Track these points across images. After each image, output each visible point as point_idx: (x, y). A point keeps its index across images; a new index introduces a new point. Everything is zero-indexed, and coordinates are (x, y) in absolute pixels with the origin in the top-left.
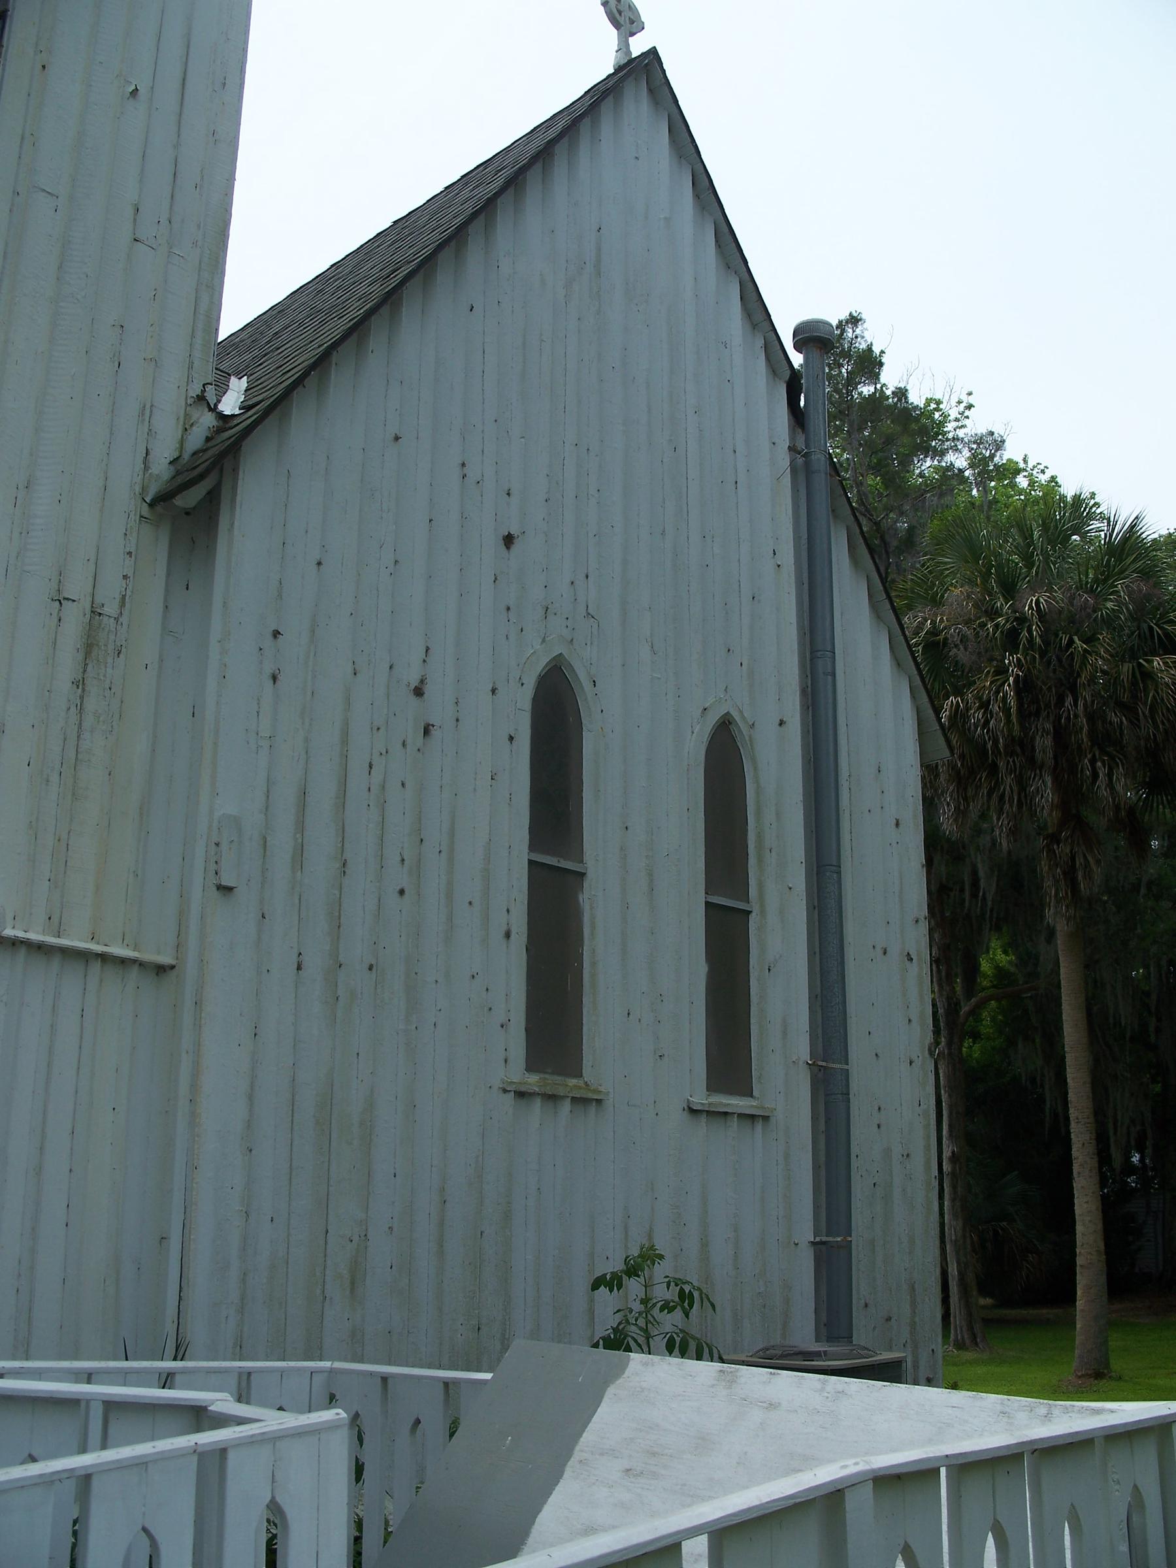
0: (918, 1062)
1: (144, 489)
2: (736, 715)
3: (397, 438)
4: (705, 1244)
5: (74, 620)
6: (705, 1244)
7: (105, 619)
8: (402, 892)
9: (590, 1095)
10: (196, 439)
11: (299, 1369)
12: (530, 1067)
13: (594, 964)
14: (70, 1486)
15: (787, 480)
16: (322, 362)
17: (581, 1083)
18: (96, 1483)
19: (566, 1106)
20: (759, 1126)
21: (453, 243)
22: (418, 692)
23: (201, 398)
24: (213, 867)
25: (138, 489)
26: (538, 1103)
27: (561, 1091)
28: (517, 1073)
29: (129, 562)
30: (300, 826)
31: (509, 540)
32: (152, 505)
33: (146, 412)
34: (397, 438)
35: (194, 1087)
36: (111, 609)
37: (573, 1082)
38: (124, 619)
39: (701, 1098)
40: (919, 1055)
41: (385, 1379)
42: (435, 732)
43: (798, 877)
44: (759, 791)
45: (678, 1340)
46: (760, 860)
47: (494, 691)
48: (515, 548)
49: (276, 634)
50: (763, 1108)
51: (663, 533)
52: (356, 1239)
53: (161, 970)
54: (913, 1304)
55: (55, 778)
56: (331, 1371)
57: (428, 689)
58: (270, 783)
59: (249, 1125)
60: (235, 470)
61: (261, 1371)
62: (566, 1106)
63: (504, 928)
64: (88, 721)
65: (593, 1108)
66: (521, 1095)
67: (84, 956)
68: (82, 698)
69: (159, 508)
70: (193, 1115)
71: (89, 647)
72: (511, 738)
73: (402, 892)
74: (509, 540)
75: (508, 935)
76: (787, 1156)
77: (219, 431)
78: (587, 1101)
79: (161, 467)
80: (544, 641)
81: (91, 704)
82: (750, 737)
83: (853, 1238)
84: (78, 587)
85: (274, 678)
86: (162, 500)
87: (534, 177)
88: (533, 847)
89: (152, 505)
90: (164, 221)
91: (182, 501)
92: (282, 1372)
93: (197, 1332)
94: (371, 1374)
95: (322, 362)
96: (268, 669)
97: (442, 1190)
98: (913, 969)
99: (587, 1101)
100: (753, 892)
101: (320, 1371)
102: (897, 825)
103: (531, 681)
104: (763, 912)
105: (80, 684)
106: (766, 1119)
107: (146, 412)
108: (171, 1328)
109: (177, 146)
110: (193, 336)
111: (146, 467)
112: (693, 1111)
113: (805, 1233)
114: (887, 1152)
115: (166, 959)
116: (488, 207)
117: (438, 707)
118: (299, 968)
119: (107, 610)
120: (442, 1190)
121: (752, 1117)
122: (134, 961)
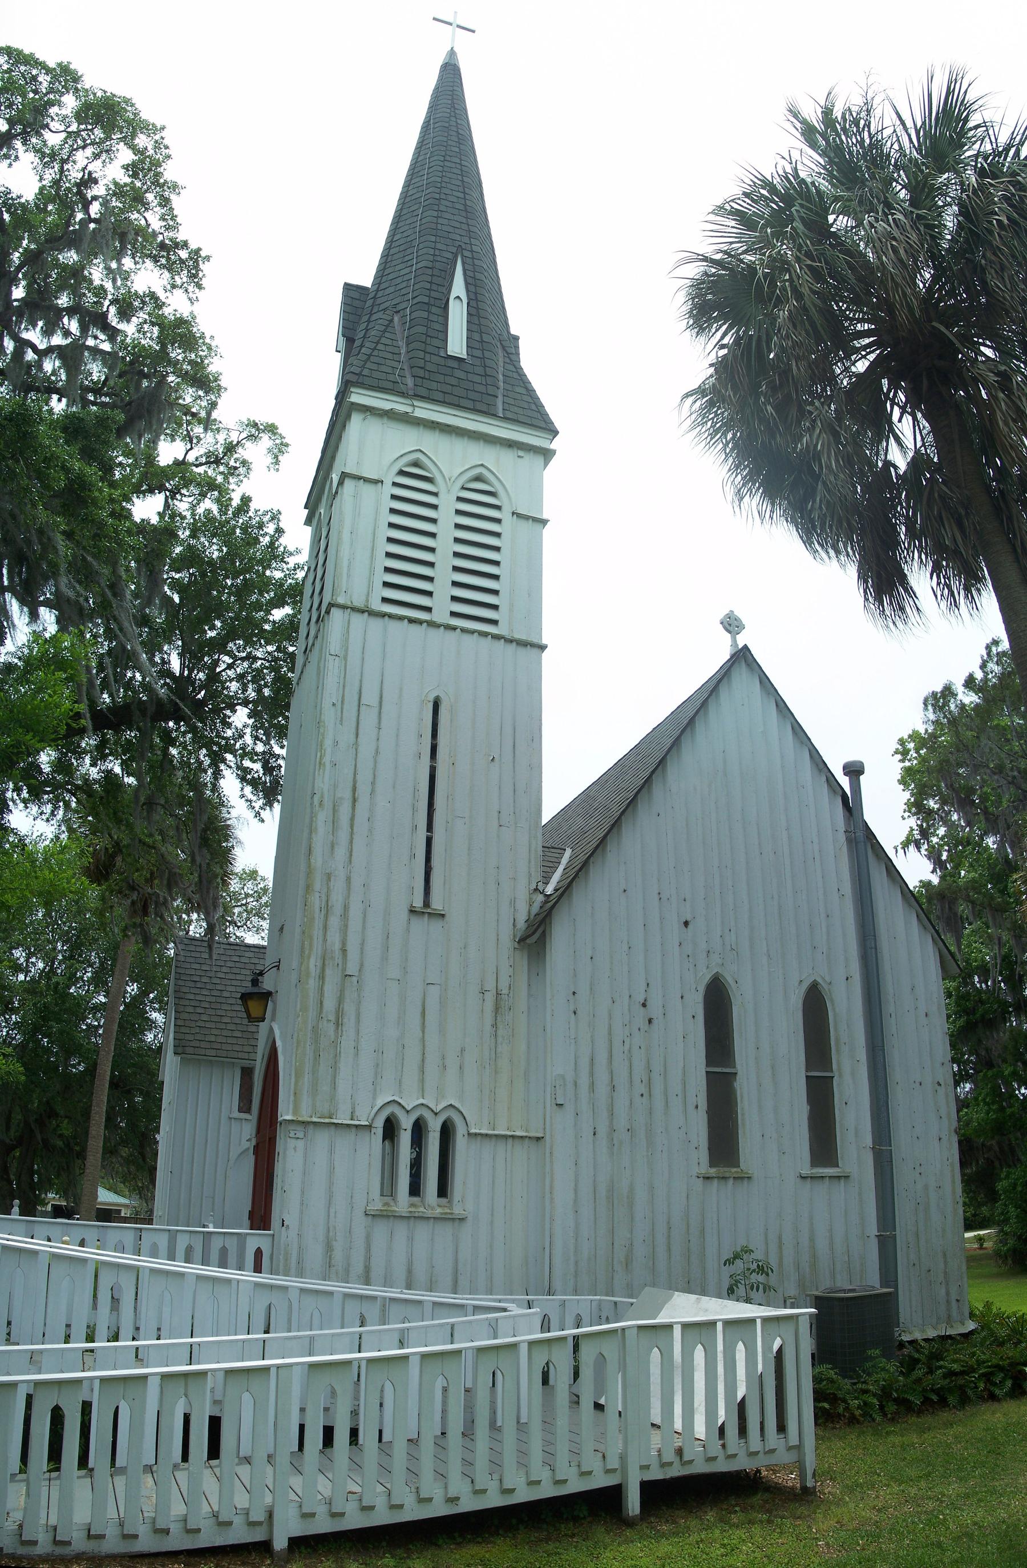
0: (945, 1138)
1: (514, 936)
2: (819, 980)
3: (625, 891)
4: (812, 1240)
5: (490, 997)
6: (812, 1240)
7: (503, 996)
8: (642, 1095)
9: (743, 1175)
10: (535, 909)
11: (585, 1300)
12: (712, 1163)
13: (743, 1115)
14: (449, 1327)
15: (845, 849)
16: (603, 841)
17: (739, 1170)
18: (456, 1327)
19: (731, 1181)
20: (842, 1181)
21: (646, 786)
22: (644, 1005)
23: (536, 890)
24: (554, 1096)
25: (512, 937)
26: (716, 1180)
27: (727, 1175)
28: (704, 1168)
29: (511, 969)
30: (592, 1074)
31: (686, 924)
32: (519, 942)
33: (513, 902)
34: (625, 891)
35: (551, 1188)
36: (505, 991)
37: (734, 1170)
38: (511, 995)
39: (806, 1171)
40: (943, 1136)
41: (615, 1303)
42: (655, 1022)
43: (862, 1055)
44: (835, 1016)
45: (755, 1285)
46: (838, 1051)
47: (682, 997)
48: (690, 926)
49: (574, 993)
50: (844, 1172)
51: (772, 898)
52: (627, 1245)
53: (538, 1139)
54: (946, 1263)
55: (487, 1066)
56: (600, 1300)
57: (648, 1003)
58: (576, 1058)
59: (575, 1201)
60: (551, 923)
61: (569, 1300)
62: (731, 1181)
63: (695, 1104)
64: (500, 1039)
65: (746, 1181)
66: (707, 1178)
67: (505, 1137)
68: (496, 1031)
69: (522, 944)
70: (552, 1199)
71: (497, 1009)
72: (694, 1017)
73: (642, 1095)
74: (686, 924)
75: (697, 1107)
76: (860, 1194)
77: (546, 902)
78: (744, 1178)
79: (521, 924)
80: (708, 967)
81: (500, 1032)
82: (829, 990)
83: (898, 1232)
84: (490, 985)
85: (575, 1013)
86: (522, 940)
87: (712, 702)
88: (707, 1065)
89: (519, 942)
90: (512, 814)
91: (528, 941)
92: (578, 1301)
93: (557, 1284)
94: (611, 1301)
95: (603, 841)
96: (572, 1008)
97: (668, 1223)
98: (941, 1091)
99: (744, 1178)
100: (834, 1066)
101: (595, 1300)
102: (926, 1015)
103: (702, 989)
104: (840, 1075)
105: (495, 1025)
106: (847, 1177)
107: (513, 902)
108: (547, 1284)
109: (514, 778)
110: (530, 862)
111: (514, 925)
112: (803, 1178)
113: (873, 1230)
114: (926, 1187)
115: (540, 1135)
116: (704, 704)
117: (655, 1009)
118: (594, 1134)
119: (503, 992)
120: (668, 1223)
121: (839, 1177)
122: (526, 1137)
